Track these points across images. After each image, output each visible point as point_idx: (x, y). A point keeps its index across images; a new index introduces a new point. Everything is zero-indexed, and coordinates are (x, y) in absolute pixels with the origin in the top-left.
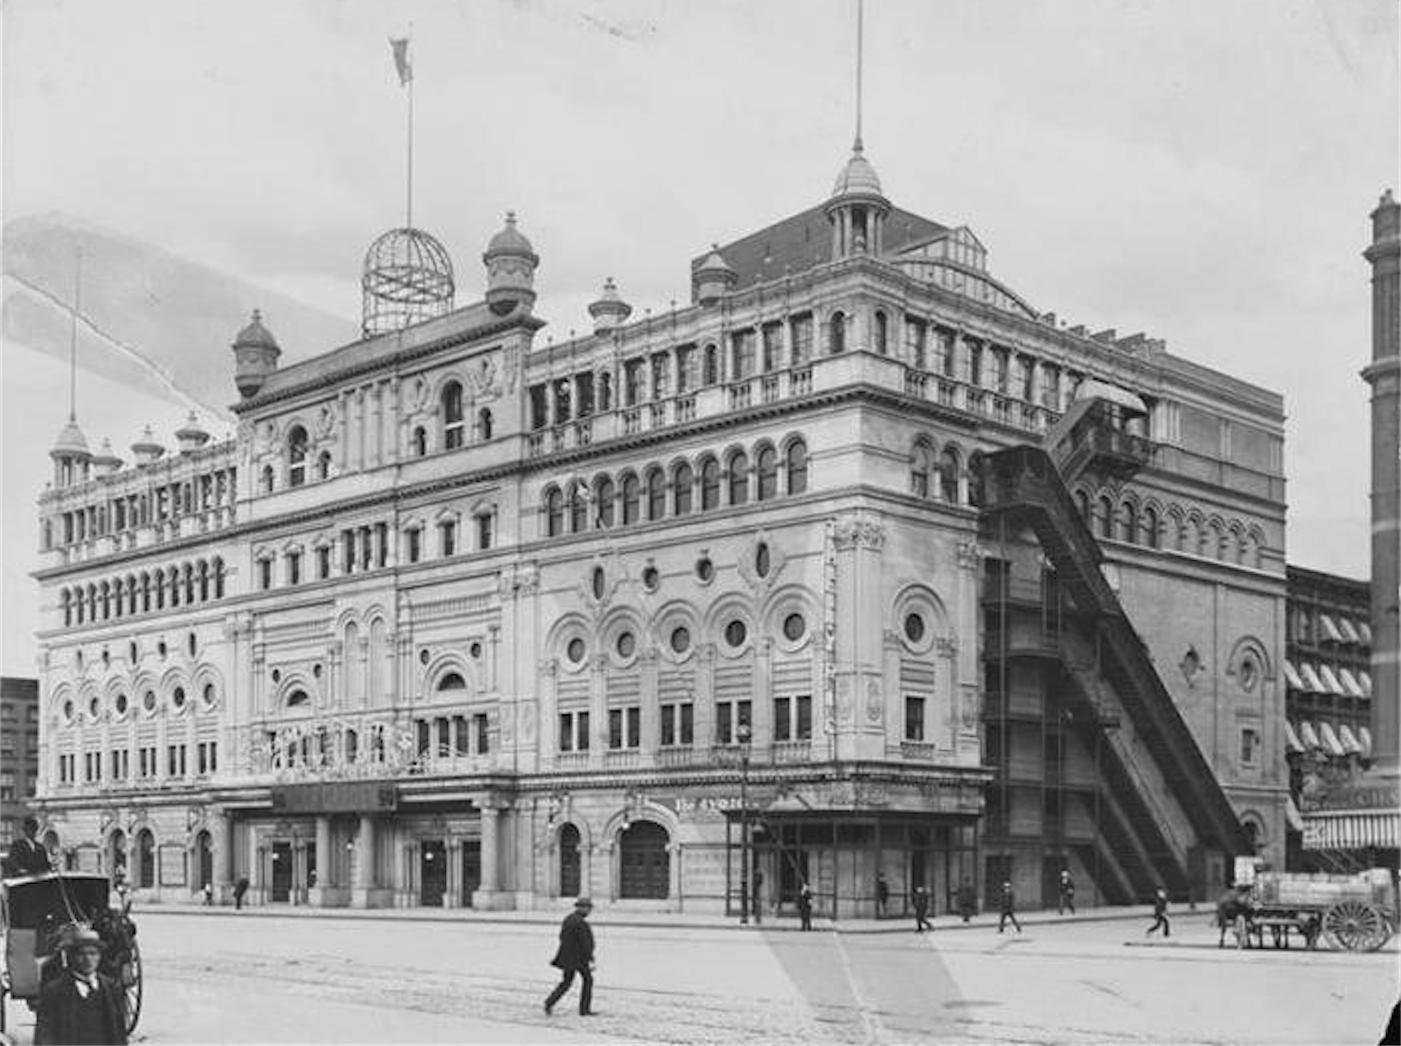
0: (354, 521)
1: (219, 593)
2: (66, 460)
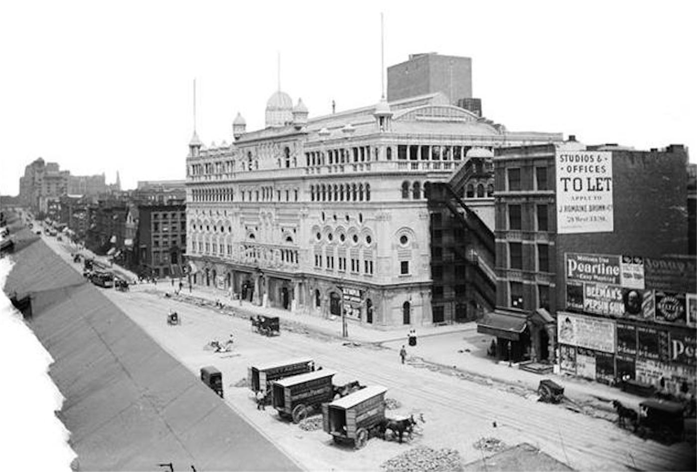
0: (265, 185)
1: (368, 199)
2: (192, 147)
